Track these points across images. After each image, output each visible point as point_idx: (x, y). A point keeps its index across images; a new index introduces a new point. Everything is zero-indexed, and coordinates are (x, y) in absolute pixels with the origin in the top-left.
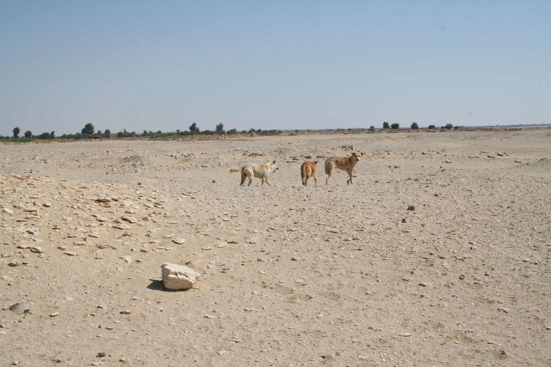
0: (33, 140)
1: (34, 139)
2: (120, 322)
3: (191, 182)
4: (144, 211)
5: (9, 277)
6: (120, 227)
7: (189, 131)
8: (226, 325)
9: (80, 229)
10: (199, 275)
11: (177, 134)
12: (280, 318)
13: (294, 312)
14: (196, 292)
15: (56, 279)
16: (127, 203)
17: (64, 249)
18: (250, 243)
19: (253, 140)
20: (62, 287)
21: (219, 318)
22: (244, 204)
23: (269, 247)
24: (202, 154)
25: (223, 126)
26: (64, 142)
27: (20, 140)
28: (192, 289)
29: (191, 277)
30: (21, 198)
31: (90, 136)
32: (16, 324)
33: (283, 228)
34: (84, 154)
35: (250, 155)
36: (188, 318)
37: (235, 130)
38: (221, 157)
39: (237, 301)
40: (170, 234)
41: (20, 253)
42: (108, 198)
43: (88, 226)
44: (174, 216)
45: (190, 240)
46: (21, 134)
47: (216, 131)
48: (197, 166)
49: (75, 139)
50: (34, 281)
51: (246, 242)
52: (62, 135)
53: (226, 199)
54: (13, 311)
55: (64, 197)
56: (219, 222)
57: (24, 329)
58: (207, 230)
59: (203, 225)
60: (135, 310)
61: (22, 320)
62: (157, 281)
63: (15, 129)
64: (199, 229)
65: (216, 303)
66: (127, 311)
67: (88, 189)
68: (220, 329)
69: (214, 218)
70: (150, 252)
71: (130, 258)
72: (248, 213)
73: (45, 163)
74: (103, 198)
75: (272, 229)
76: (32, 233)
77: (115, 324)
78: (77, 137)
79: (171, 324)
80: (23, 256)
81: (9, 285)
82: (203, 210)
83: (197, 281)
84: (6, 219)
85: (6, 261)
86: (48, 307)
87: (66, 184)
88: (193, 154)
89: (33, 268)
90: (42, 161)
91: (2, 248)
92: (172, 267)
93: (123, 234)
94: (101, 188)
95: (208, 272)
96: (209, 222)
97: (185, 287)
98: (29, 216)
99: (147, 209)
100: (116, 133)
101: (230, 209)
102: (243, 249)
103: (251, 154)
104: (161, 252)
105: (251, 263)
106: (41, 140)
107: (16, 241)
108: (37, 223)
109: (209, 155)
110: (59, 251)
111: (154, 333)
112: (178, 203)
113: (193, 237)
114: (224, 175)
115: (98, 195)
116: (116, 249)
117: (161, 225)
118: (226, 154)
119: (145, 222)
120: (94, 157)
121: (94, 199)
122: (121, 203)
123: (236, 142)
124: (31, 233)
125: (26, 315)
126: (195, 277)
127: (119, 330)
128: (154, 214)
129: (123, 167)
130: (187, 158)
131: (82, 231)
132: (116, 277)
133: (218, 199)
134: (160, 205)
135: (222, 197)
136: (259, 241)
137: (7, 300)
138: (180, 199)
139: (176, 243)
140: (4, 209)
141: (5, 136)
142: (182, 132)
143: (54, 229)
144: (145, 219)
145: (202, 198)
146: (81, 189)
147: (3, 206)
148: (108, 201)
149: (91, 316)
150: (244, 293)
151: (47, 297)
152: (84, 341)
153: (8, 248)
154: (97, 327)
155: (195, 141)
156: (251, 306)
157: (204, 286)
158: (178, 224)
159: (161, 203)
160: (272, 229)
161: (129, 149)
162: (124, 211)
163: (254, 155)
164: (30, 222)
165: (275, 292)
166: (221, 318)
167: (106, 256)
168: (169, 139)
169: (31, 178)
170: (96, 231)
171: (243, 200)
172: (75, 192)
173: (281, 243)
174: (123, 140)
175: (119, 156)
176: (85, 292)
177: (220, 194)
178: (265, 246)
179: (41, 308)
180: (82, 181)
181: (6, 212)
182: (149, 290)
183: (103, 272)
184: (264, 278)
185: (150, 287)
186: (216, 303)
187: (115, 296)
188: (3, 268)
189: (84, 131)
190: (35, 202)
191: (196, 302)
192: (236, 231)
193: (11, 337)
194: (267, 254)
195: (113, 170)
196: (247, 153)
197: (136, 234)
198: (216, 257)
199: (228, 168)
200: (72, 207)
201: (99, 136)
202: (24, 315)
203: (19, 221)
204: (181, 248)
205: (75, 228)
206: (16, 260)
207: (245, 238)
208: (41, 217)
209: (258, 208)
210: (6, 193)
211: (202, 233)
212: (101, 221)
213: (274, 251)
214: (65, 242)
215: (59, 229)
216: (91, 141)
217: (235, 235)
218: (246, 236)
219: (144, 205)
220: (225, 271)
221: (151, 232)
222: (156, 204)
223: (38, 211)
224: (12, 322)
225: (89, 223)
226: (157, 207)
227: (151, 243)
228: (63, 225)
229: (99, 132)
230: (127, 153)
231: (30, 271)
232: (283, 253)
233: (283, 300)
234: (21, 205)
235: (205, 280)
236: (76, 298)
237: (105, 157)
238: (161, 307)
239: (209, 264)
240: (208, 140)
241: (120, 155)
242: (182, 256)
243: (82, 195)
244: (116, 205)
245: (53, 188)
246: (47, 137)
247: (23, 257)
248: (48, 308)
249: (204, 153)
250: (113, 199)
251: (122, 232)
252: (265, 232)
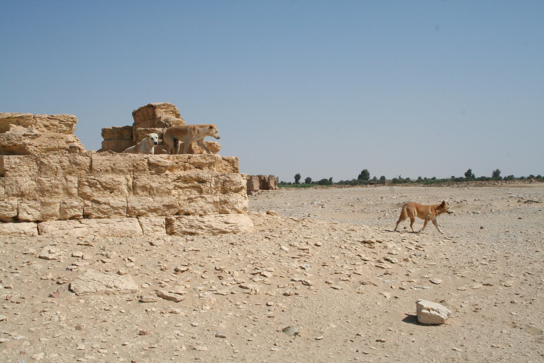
0: (312, 186)
1: (313, 185)
2: (375, 348)
3: (459, 228)
4: (405, 253)
5: (283, 304)
6: (382, 266)
7: (464, 177)
8: (472, 358)
9: (346, 266)
10: (450, 312)
11: (452, 181)
12: (525, 355)
13: (540, 351)
14: (447, 327)
15: (322, 308)
16: (390, 245)
17: (331, 283)
18: (505, 286)
19: (532, 187)
20: (327, 316)
21: (466, 351)
22: (504, 249)
23: (524, 290)
24: (475, 200)
25: (500, 173)
26: (342, 188)
27: (301, 186)
28: (443, 325)
29: (443, 314)
30: (296, 238)
31: (366, 181)
32: (287, 343)
33: (540, 274)
34: (359, 200)
35: (525, 202)
36: (437, 349)
37: (512, 176)
38: (495, 203)
39: (485, 337)
40: (428, 275)
41: (293, 285)
42: (373, 240)
43: (353, 265)
44: (434, 259)
45: (446, 281)
46: (302, 180)
47: (493, 177)
48: (468, 212)
49: (352, 185)
50: (303, 309)
51: (501, 285)
52: (480, 177)
53: (487, 244)
54: (286, 333)
55: (334, 238)
56: (477, 265)
57: (294, 348)
58: (464, 272)
59: (461, 267)
60: (390, 339)
61: (292, 340)
62: (412, 316)
63: (296, 175)
64: (456, 271)
65: (464, 338)
66: (382, 339)
67: (356, 232)
68: (466, 361)
69: (472, 262)
70: (408, 290)
71: (389, 294)
72: (507, 257)
73: (322, 207)
74: (368, 240)
75: (529, 274)
76: (304, 269)
77: (371, 350)
78: (353, 183)
79: (421, 353)
80: (295, 288)
81: (283, 311)
82: (463, 254)
83: (448, 318)
84: (282, 256)
85: (281, 291)
86: (315, 331)
87: (336, 227)
88: (466, 201)
89: (303, 298)
90: (320, 206)
91: (279, 280)
92: (426, 304)
93: (384, 273)
94: (368, 231)
95: (460, 311)
96: (467, 265)
97: (437, 322)
98: (302, 254)
99: (408, 251)
100: (391, 179)
101: (490, 254)
102: (497, 291)
103: (526, 201)
104: (418, 290)
105: (504, 304)
106: (319, 185)
107: (290, 275)
108: (309, 260)
109: (482, 201)
110: (327, 285)
111: (405, 360)
112: (439, 246)
113: (450, 278)
114: (494, 222)
115: (364, 237)
116: (377, 286)
117: (420, 266)
118: (500, 201)
119: (406, 263)
120: (368, 202)
121: (360, 241)
122: (385, 244)
123: (513, 188)
124: (303, 268)
125: (295, 337)
126: (447, 314)
127: (374, 355)
128: (415, 255)
129: (395, 213)
130: (459, 204)
131: (347, 269)
132: (375, 309)
133: (479, 244)
134: (421, 248)
135: (484, 242)
136: (514, 285)
137: (281, 323)
138: (442, 243)
139: (433, 283)
140: (282, 247)
141: (287, 182)
142: (457, 179)
143: (323, 266)
144: (406, 260)
145: (464, 242)
146: (349, 231)
147: (281, 245)
148: (373, 243)
149: (350, 342)
150: (493, 331)
151: (314, 323)
152: (343, 361)
153: (284, 280)
154: (355, 351)
155: (470, 188)
156: (498, 343)
157: (455, 323)
158: (437, 266)
159: (422, 246)
160: (529, 274)
161: (403, 195)
162: (387, 252)
163: (530, 202)
164: (302, 259)
165: (524, 332)
166: (468, 351)
167: (368, 292)
168: (443, 185)
169: (306, 220)
170: (360, 269)
171: (504, 246)
172: (344, 233)
173: (537, 287)
174: (398, 186)
175: (392, 202)
176: (347, 321)
177: (482, 239)
178: (520, 289)
179: (309, 332)
180: (352, 224)
181: (283, 249)
182: (404, 323)
183: (363, 305)
184: (515, 319)
185: (405, 320)
186: (464, 338)
187: (373, 326)
188: (278, 296)
189: (360, 177)
190: (308, 241)
191: (446, 336)
192: (492, 275)
193: (283, 354)
194: (521, 297)
195: (385, 215)
196: (522, 200)
197: (397, 274)
198: (470, 297)
199: (500, 214)
200: (340, 247)
201: (375, 182)
202: (294, 336)
203: (294, 258)
204: (437, 288)
205: (341, 265)
206: (289, 290)
207: (501, 281)
208: (312, 255)
209: (518, 254)
210: (283, 233)
211: (459, 274)
212: (365, 260)
213: (528, 295)
214: (332, 278)
215: (327, 266)
216: (366, 187)
217: (491, 278)
218: (502, 279)
219: (406, 247)
220: (477, 310)
221: (410, 272)
222: (417, 247)
223: (310, 249)
224: (284, 342)
225: (354, 262)
226: (418, 249)
227: (410, 282)
228: (331, 263)
229: (375, 178)
230: (400, 199)
231: (301, 301)
232: (538, 297)
233: (531, 340)
234: (296, 244)
235: (457, 317)
236: (339, 326)
237: (379, 202)
238: (413, 338)
239: (462, 303)
240: (483, 186)
241: (394, 200)
242: (438, 295)
243: (350, 236)
244: (380, 246)
245: (324, 230)
246: (325, 183)
247: (296, 289)
248: (315, 333)
249: (477, 199)
250: (377, 241)
251: (384, 271)
252: (521, 277)
